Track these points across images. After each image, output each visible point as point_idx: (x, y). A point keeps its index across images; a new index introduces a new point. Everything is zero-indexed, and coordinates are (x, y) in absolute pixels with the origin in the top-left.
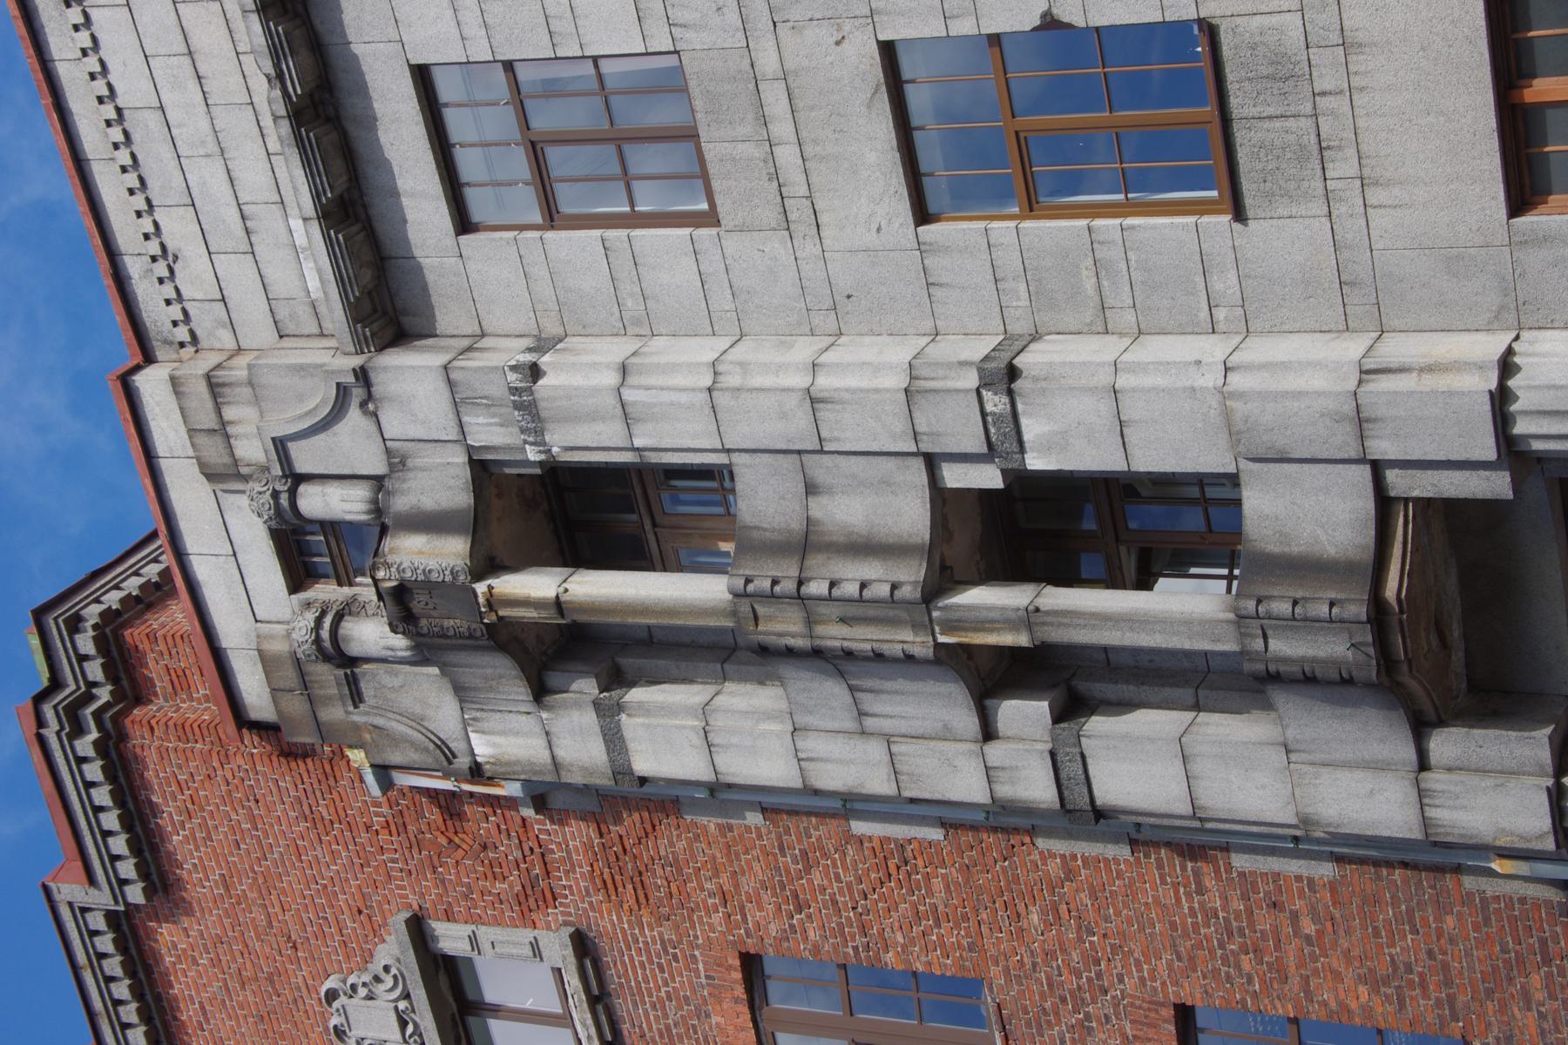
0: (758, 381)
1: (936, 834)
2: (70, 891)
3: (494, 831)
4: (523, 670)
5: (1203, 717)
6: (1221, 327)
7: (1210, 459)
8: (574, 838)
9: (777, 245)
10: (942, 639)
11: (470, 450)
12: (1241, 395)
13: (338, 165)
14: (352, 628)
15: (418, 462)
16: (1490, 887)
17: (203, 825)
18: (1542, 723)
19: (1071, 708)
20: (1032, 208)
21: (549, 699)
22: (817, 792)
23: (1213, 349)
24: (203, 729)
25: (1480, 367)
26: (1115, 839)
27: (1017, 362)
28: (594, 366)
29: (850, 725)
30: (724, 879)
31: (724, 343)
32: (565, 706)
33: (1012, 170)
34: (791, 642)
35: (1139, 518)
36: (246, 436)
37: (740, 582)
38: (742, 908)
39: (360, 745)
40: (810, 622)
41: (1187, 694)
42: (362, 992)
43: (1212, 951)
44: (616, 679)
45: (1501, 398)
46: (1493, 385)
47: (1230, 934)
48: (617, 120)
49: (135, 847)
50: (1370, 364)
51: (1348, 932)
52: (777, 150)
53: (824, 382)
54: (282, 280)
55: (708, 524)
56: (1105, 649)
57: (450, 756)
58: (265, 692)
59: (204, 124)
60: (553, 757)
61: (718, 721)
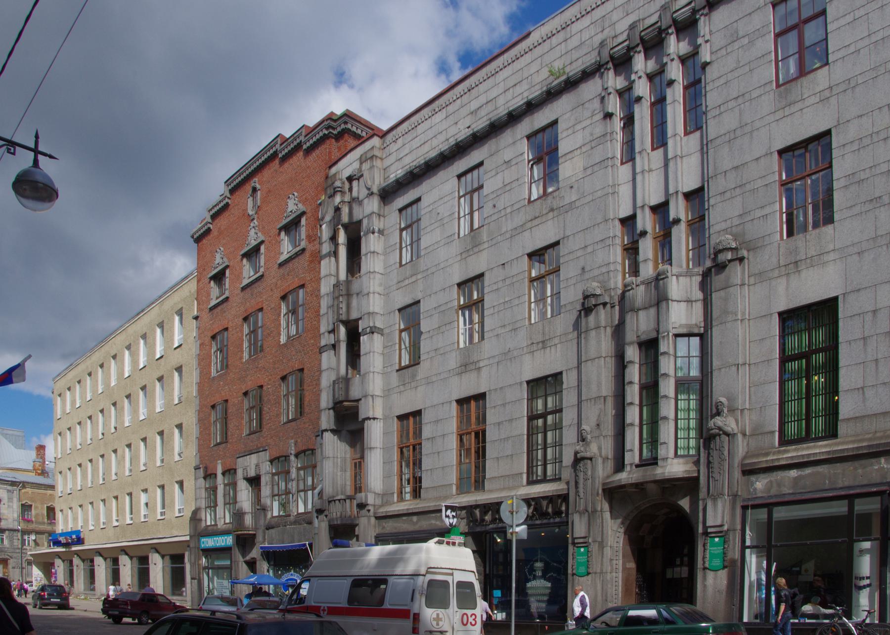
7: (362, 372)
9: (395, 281)
25: (373, 415)
28: (374, 246)
45: (369, 419)
46: (371, 417)
53: (371, 295)
54: (393, 168)
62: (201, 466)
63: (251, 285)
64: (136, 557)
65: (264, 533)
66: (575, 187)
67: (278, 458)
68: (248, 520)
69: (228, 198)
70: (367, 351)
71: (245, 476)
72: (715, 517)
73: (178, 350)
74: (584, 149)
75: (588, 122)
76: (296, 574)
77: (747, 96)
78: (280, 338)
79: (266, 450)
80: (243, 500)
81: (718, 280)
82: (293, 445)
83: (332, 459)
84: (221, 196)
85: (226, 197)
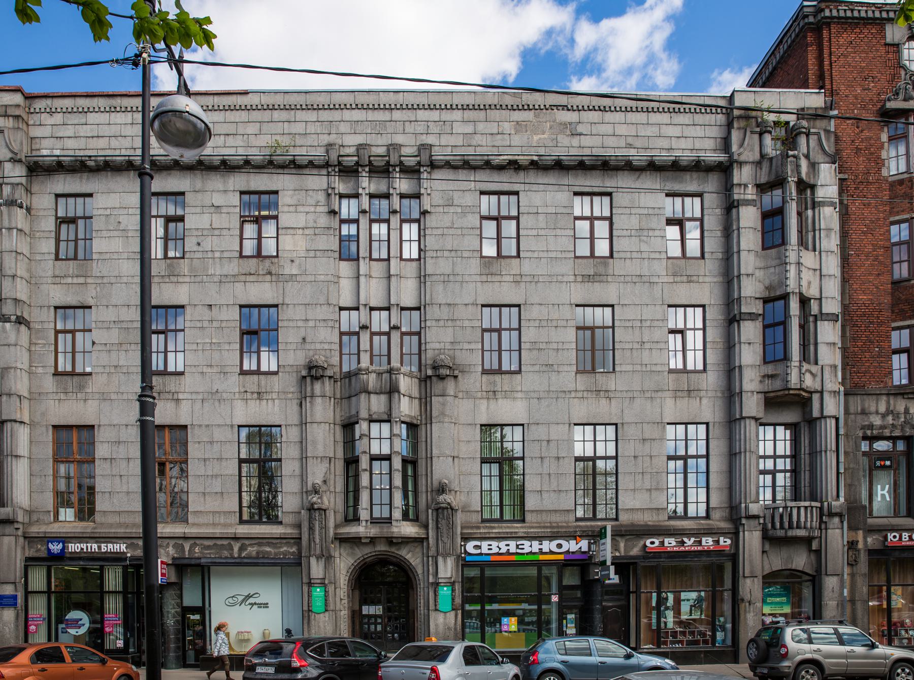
9: (50, 273)
59: (82, 134)
66: (297, 261)
72: (446, 571)
74: (307, 232)
75: (312, 209)
77: (459, 253)
81: (437, 387)
84: (172, 69)
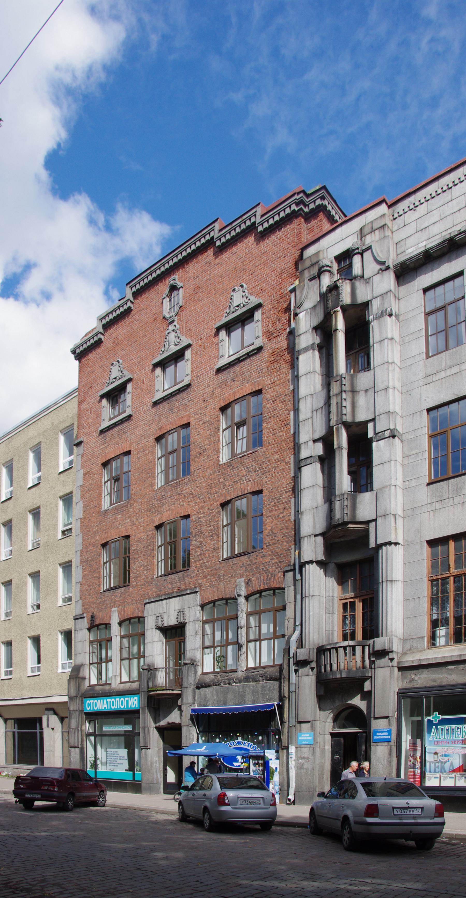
0: (390, 374)
1: (292, 432)
2: (259, 211)
3: (283, 322)
4: (320, 323)
5: (322, 489)
6: (404, 483)
8: (284, 344)
9: (422, 375)
10: (334, 427)
11: (371, 300)
12: (390, 489)
13: (439, 253)
14: (327, 274)
15: (368, 287)
16: (293, 551)
17: (278, 244)
18: (325, 558)
19: (321, 459)
20: (431, 436)
21: (314, 331)
22: (299, 402)
23: (400, 482)
24: (300, 239)
25: (396, 539)
26: (295, 473)
27: (396, 437)
29: (314, 408)
30: (278, 382)
31: (399, 364)
32: (313, 336)
33: (439, 431)
34: (331, 391)
35: (363, 471)
36: (371, 238)
37: (344, 376)
38: (272, 388)
39: (300, 283)
40: (336, 395)
41: (326, 485)
42: (244, 294)
43: (274, 496)
44: (320, 347)
45: (390, 543)
46: (393, 542)
47: (278, 500)
48: (451, 329)
49: (271, 226)
50: (397, 516)
51: (281, 524)
52: (443, 372)
53: (390, 391)
54: (410, 242)
55: (357, 366)
56: (334, 466)
57: (299, 307)
58: (310, 255)
59: (448, 213)
60: (301, 334)
61: (312, 375)
62: (85, 615)
63: (169, 398)
64: (14, 719)
65: (194, 693)
67: (129, 619)
68: (161, 679)
69: (131, 302)
70: (386, 458)
71: (160, 624)
73: (34, 489)
76: (247, 743)
78: (218, 457)
79: (197, 592)
80: (155, 654)
82: (243, 584)
83: (317, 598)
85: (128, 300)
